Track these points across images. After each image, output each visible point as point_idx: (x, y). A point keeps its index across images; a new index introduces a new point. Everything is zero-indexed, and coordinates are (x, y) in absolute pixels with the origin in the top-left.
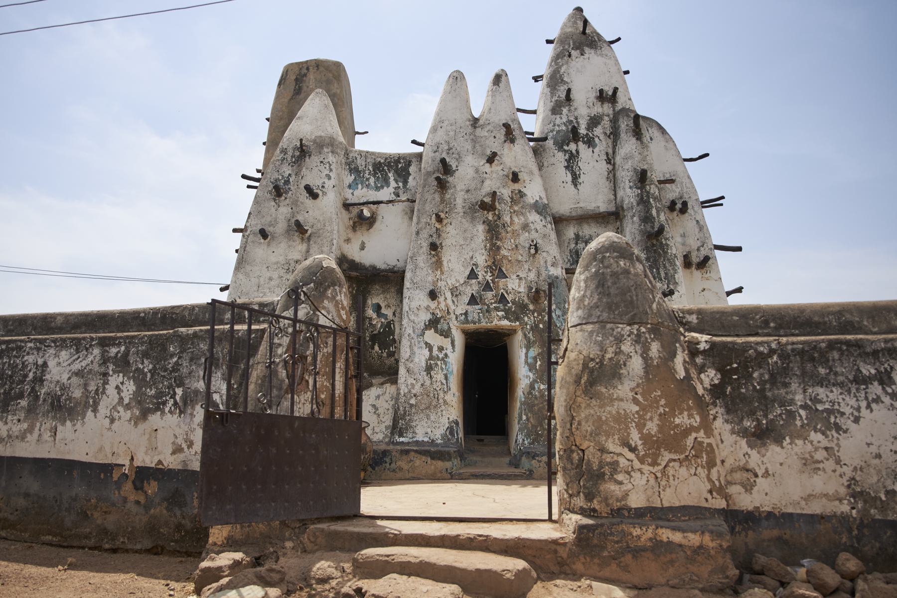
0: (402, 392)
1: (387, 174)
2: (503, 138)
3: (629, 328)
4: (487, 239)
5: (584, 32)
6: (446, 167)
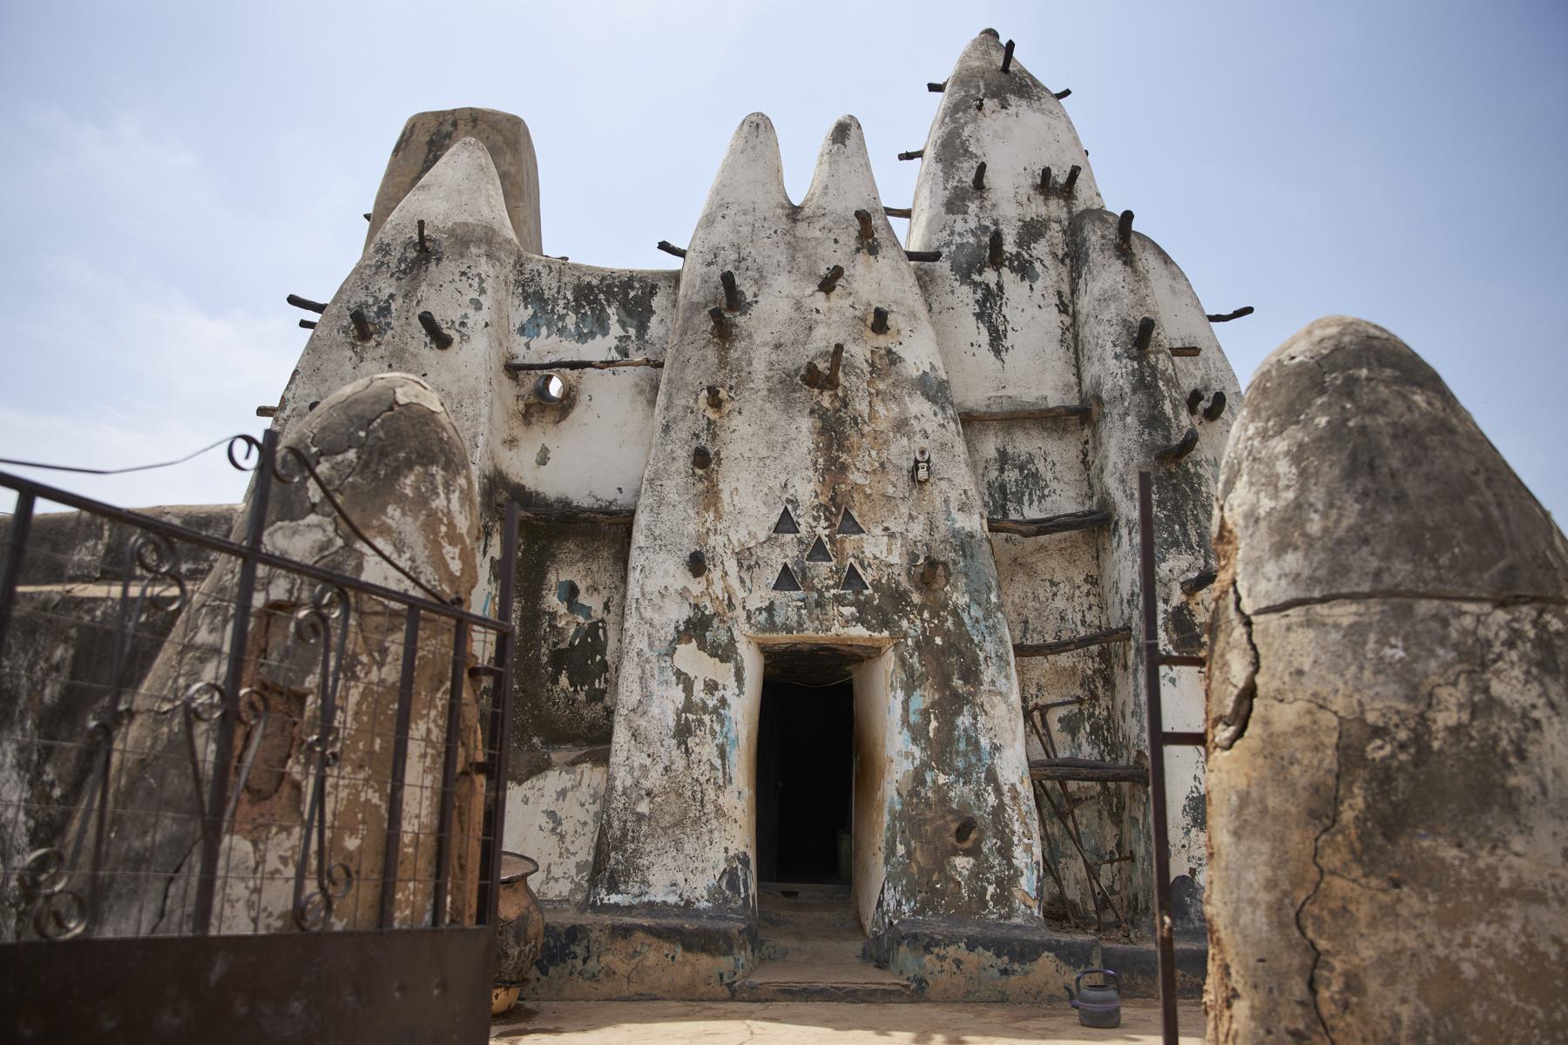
0: (618, 783)
1: (603, 310)
2: (853, 244)
3: (1501, 616)
4: (818, 449)
5: (1005, 69)
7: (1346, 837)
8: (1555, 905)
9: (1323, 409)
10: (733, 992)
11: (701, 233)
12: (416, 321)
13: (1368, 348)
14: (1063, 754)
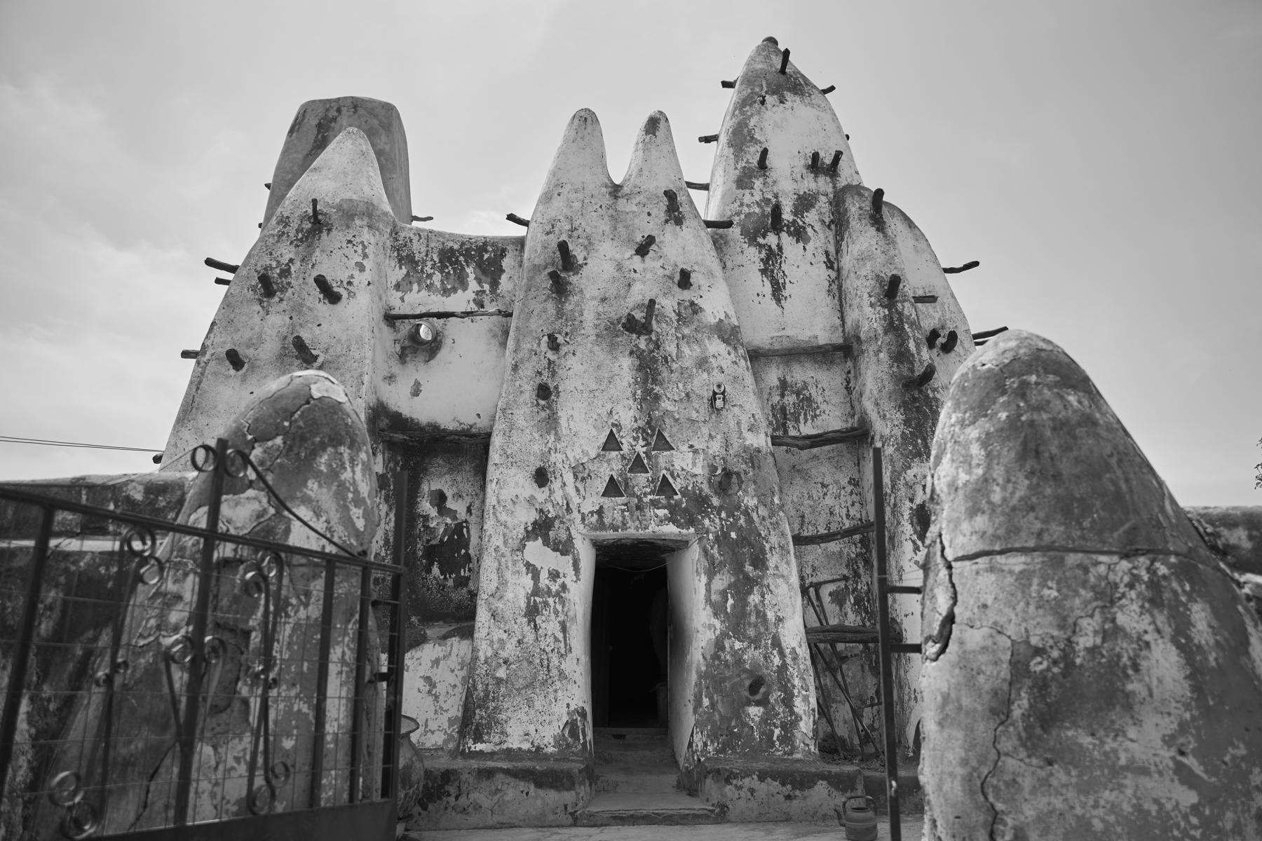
0: (481, 655)
1: (463, 269)
2: (663, 216)
3: (1125, 565)
4: (636, 383)
5: (783, 71)
6: (566, 260)
7: (1016, 728)
8: (1156, 776)
9: (1005, 406)
10: (575, 819)
11: (541, 207)
12: (311, 281)
13: (1037, 358)
14: (833, 621)
